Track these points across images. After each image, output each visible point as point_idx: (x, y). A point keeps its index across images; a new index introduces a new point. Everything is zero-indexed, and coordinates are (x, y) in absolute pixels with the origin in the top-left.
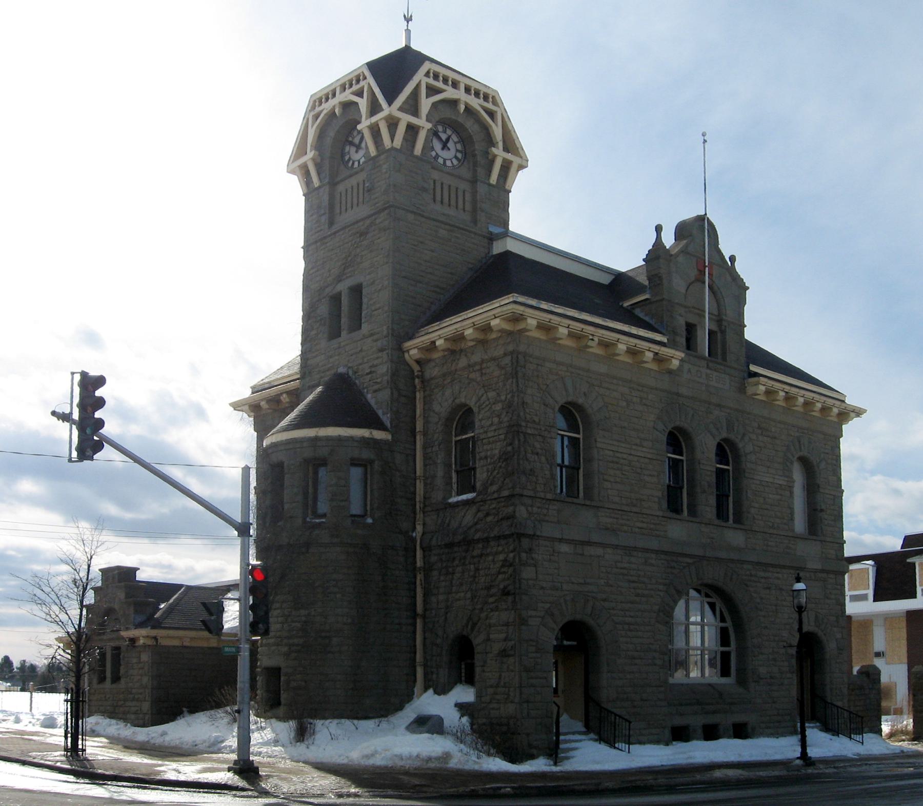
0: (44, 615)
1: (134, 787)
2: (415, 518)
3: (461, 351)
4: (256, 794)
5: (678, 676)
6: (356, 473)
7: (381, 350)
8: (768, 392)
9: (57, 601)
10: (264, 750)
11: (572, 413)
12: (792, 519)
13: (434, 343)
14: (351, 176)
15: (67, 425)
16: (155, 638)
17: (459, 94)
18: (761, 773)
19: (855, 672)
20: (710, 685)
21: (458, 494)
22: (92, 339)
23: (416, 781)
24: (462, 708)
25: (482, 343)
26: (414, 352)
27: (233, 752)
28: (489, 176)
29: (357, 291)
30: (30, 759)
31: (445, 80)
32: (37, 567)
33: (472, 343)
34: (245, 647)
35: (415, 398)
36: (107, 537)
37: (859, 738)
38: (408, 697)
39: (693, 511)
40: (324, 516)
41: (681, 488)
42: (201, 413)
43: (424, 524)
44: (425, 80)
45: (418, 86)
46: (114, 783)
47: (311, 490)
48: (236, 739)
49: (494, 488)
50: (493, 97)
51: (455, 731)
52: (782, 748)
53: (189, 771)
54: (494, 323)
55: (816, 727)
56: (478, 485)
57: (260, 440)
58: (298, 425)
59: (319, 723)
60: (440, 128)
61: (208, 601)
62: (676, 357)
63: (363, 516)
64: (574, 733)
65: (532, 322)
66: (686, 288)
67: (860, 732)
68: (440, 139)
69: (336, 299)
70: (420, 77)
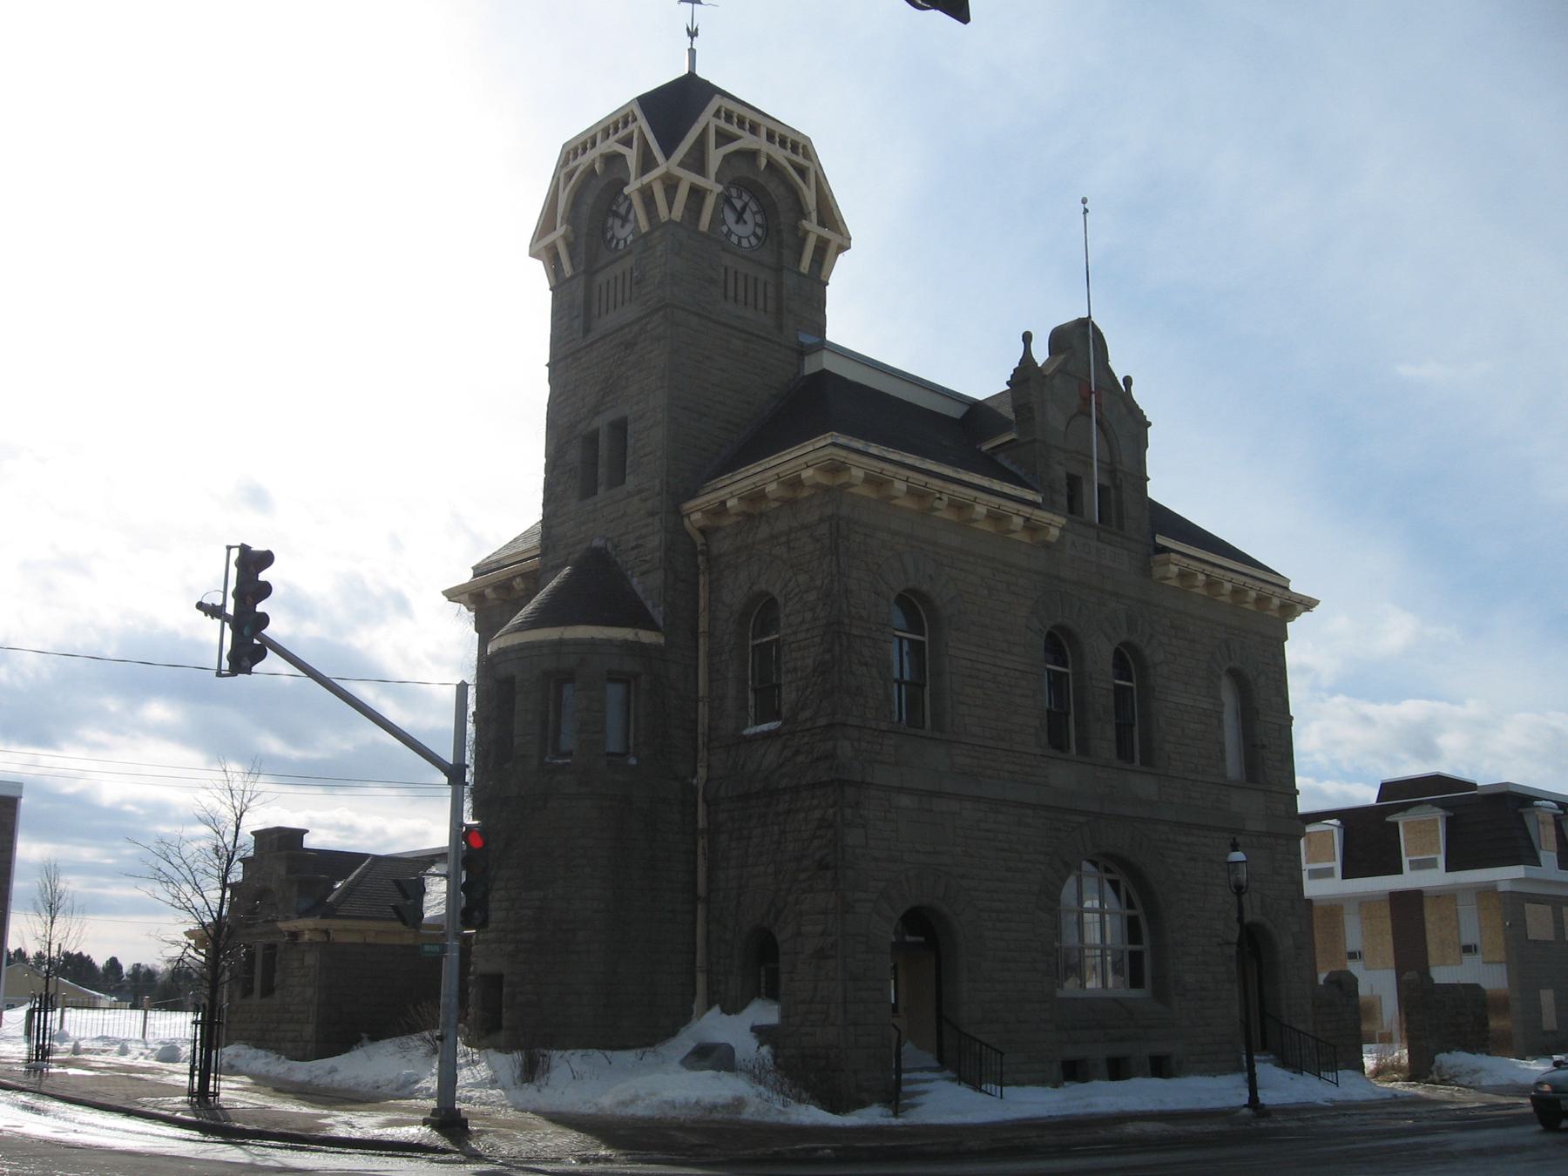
0: (169, 899)
1: (286, 1148)
2: (696, 757)
3: (761, 515)
4: (463, 1158)
5: (1070, 987)
6: (615, 692)
7: (652, 514)
8: (1184, 575)
9: (190, 878)
10: (476, 1094)
11: (913, 605)
12: (1223, 760)
13: (723, 503)
14: (613, 262)
15: (218, 622)
16: (326, 932)
17: (759, 143)
18: (1193, 1128)
19: (1321, 982)
20: (1115, 1000)
21: (757, 723)
22: (257, 498)
23: (694, 1140)
24: (762, 1033)
25: (790, 503)
26: (696, 516)
27: (430, 1096)
28: (799, 261)
29: (620, 428)
30: (139, 1108)
31: (741, 123)
32: (164, 829)
33: (777, 504)
34: (454, 945)
35: (698, 584)
36: (263, 785)
37: (1331, 1076)
38: (684, 1017)
39: (1083, 747)
40: (569, 754)
41: (1067, 714)
42: (402, 605)
43: (709, 767)
44: (714, 122)
45: (705, 130)
46: (258, 1142)
47: (551, 717)
48: (436, 1078)
49: (807, 714)
50: (804, 147)
51: (750, 1066)
52: (1218, 1091)
53: (367, 1124)
54: (807, 474)
55: (1270, 1061)
56: (784, 710)
57: (483, 644)
58: (532, 623)
59: (556, 1055)
60: (734, 192)
61: (403, 875)
62: (1054, 524)
63: (624, 755)
64: (921, 1070)
65: (858, 474)
66: (1072, 408)
67: (1334, 1068)
68: (733, 207)
69: (591, 440)
70: (707, 118)
